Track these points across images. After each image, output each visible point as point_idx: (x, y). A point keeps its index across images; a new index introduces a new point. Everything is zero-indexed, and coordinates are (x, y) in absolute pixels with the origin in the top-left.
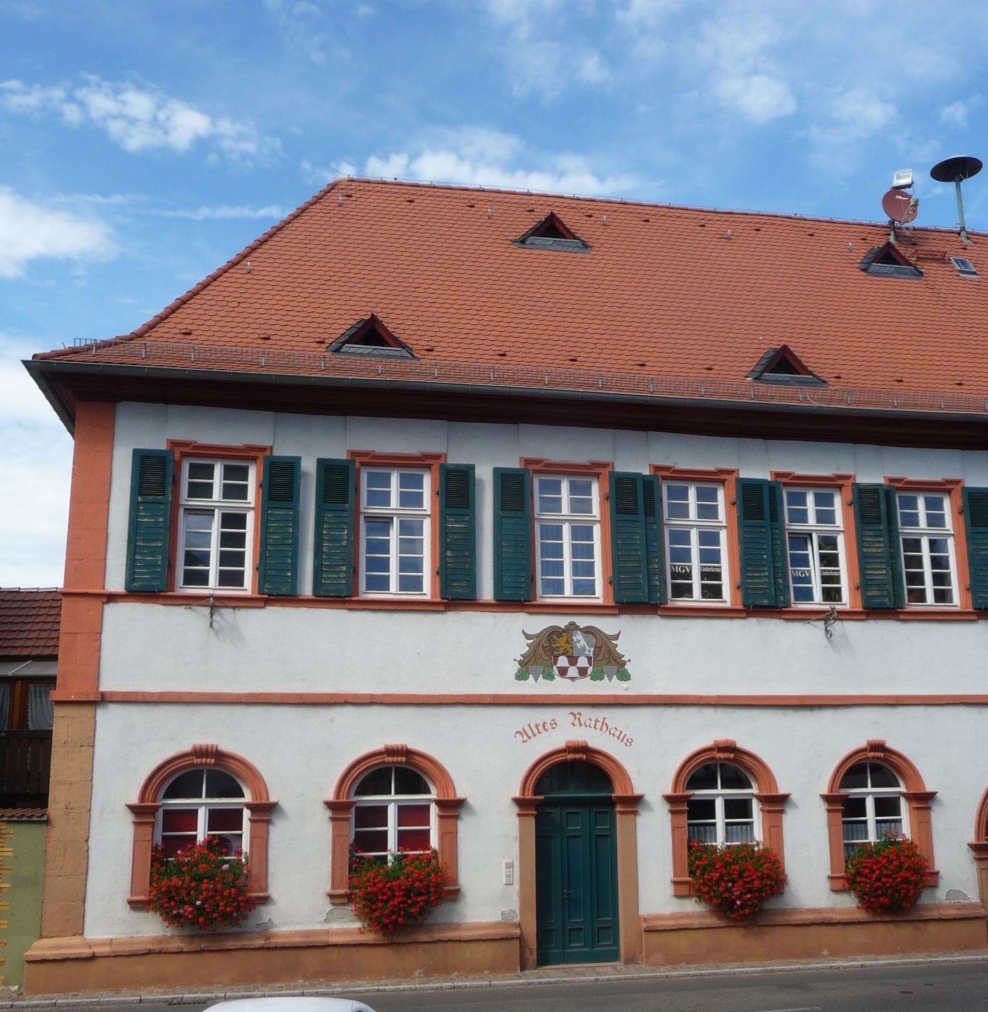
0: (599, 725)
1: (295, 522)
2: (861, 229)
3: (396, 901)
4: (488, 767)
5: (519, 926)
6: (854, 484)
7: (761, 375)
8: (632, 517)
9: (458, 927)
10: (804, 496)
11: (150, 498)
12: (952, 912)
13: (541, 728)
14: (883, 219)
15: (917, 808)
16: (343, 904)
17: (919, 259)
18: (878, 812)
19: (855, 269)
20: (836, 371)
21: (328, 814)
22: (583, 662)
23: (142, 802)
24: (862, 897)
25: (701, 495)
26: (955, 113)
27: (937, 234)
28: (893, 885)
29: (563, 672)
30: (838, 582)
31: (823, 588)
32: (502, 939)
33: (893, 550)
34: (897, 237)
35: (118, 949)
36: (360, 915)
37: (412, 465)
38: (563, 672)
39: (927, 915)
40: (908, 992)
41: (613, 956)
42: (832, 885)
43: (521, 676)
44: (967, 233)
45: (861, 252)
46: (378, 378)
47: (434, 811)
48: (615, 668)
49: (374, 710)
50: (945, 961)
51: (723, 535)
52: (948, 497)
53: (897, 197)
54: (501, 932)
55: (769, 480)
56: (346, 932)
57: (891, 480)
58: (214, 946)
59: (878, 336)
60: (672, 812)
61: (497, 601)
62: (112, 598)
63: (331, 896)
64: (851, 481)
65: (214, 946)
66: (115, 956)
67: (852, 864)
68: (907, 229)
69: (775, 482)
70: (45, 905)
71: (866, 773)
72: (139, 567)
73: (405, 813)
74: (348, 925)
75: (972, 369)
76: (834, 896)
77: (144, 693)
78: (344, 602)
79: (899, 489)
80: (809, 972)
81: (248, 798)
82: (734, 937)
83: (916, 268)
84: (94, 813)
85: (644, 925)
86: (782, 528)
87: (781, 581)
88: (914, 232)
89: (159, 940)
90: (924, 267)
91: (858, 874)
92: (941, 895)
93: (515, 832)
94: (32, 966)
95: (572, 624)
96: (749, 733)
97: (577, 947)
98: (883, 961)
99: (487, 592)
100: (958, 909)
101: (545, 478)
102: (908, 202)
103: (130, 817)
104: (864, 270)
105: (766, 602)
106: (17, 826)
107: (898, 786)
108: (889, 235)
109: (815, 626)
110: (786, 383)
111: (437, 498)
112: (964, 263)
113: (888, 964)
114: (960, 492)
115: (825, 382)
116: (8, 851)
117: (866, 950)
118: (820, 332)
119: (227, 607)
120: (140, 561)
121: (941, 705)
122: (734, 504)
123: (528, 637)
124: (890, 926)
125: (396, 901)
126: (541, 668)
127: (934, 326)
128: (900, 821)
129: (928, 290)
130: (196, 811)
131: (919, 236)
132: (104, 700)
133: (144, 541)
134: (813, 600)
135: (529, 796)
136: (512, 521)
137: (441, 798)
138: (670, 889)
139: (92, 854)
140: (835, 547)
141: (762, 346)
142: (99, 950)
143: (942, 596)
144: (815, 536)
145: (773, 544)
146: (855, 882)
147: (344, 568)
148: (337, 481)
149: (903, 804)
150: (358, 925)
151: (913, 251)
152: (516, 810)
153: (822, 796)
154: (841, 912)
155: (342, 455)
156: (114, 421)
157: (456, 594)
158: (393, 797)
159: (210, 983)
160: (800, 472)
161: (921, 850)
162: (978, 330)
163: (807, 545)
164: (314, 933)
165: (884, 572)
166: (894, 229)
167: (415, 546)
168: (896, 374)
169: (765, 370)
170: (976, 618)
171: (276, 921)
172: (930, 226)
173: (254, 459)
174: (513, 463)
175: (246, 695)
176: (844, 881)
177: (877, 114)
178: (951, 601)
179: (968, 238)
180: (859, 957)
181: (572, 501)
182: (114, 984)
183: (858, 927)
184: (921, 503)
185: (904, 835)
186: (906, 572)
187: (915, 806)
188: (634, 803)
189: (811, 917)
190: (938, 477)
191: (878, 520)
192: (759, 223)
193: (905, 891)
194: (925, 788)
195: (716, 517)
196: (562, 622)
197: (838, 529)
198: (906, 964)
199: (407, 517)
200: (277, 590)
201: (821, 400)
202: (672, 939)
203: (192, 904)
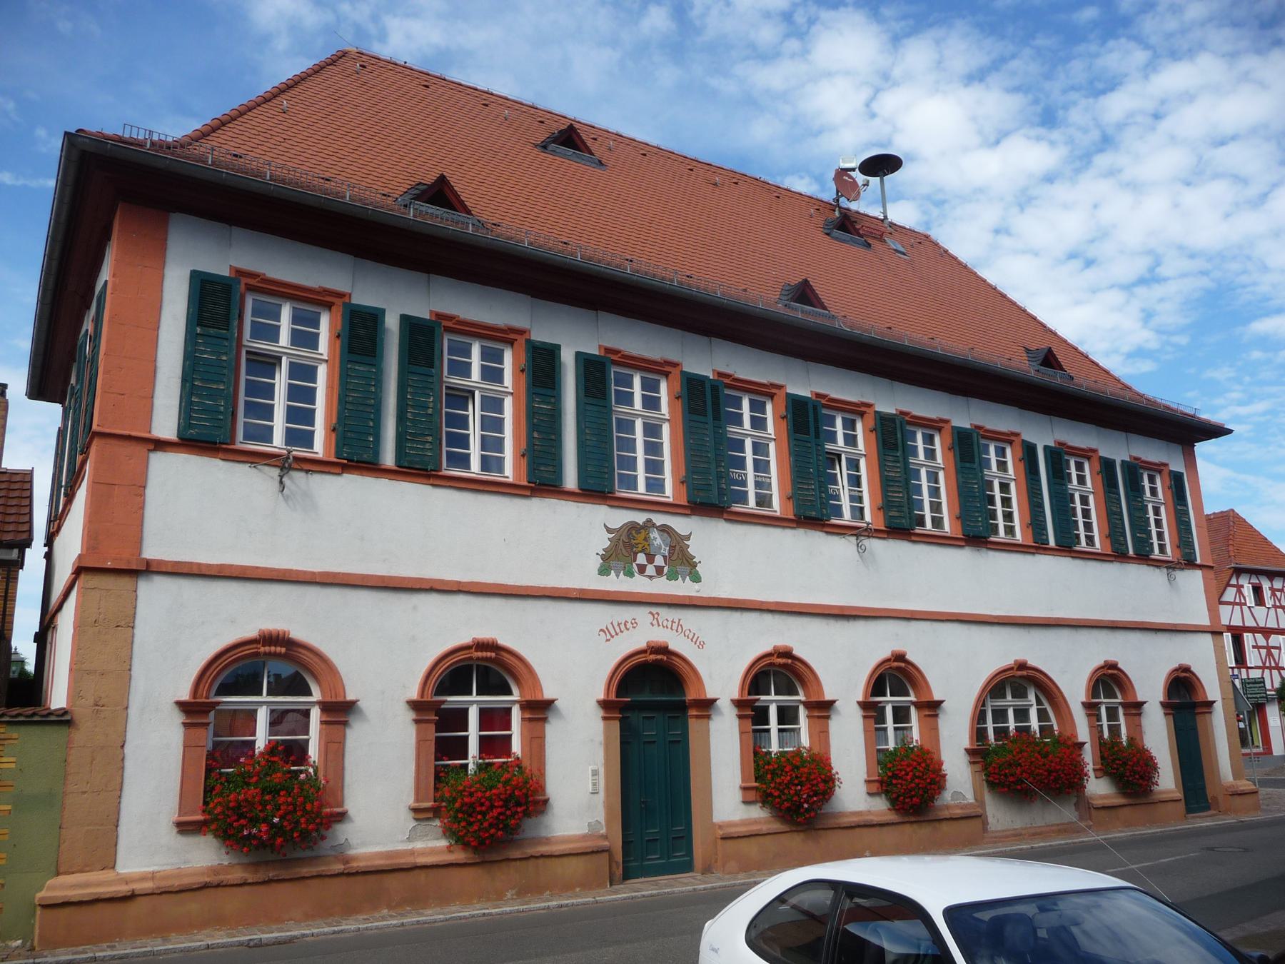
0: (675, 626)
1: (378, 380)
3: (495, 812)
4: (574, 663)
5: (605, 837)
8: (702, 419)
9: (547, 841)
11: (212, 331)
12: (958, 812)
13: (622, 627)
16: (428, 819)
21: (411, 715)
22: (659, 561)
29: (642, 569)
32: (593, 852)
35: (165, 884)
36: (448, 832)
37: (310, 301)
38: (642, 569)
41: (687, 867)
42: (744, 796)
43: (604, 571)
48: (688, 569)
49: (461, 599)
51: (322, 371)
54: (590, 845)
56: (433, 851)
58: (284, 874)
60: (740, 717)
62: (160, 445)
63: (415, 810)
65: (284, 874)
66: (161, 893)
70: (63, 831)
72: (197, 412)
73: (277, 719)
74: (432, 843)
77: (199, 565)
78: (429, 477)
81: (317, 695)
82: (796, 841)
84: (133, 712)
85: (721, 833)
86: (442, 381)
89: (214, 870)
91: (894, 776)
92: (947, 797)
93: (600, 737)
94: (49, 912)
95: (649, 521)
96: (806, 641)
97: (654, 859)
99: (571, 480)
103: (178, 718)
105: (813, 514)
106: (23, 729)
111: (338, 343)
116: (9, 762)
119: (301, 470)
120: (198, 404)
122: (522, 371)
123: (609, 530)
124: (915, 826)
125: (495, 812)
126: (621, 564)
130: (467, 710)
132: (149, 569)
133: (201, 380)
135: (613, 697)
136: (595, 408)
137: (328, 699)
138: (738, 795)
139: (128, 764)
142: (139, 887)
147: (430, 439)
148: (421, 339)
149: (802, 712)
150: (443, 843)
152: (601, 713)
156: (166, 233)
157: (541, 481)
158: (474, 697)
159: (279, 920)
164: (397, 854)
171: (353, 841)
173: (329, 306)
181: (484, 368)
182: (162, 929)
184: (476, 351)
188: (707, 705)
189: (855, 819)
190: (933, 416)
191: (895, 448)
194: (1135, 695)
196: (640, 518)
199: (492, 392)
200: (355, 456)
202: (743, 845)
203: (266, 820)
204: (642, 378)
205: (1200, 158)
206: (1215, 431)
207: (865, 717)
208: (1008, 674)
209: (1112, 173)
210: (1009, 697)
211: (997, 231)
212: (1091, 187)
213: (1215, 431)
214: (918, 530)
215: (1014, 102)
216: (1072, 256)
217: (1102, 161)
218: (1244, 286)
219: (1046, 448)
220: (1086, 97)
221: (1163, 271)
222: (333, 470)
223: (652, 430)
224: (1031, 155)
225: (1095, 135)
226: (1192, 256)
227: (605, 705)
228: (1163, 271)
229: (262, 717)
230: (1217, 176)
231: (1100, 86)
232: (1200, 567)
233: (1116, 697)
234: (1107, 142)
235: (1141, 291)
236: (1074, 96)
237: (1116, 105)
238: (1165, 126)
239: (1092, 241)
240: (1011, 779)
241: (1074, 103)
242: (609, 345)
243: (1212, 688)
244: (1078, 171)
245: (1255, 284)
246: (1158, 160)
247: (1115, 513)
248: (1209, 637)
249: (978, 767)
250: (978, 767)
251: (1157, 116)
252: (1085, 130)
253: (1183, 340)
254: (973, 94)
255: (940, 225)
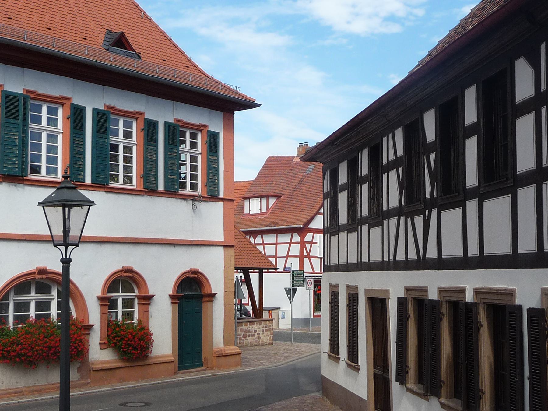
46: (53, 49)
47: (136, 301)
57: (28, 91)
60: (101, 305)
75: (20, 10)
78: (104, 188)
79: (32, 98)
99: (161, 188)
114: (69, 106)
148: (174, 133)
149: (136, 301)
153: (98, 297)
155: (19, 90)
160: (41, 91)
184: (44, 109)
204: (48, 107)
206: (249, 105)
207: (172, 303)
208: (30, 277)
210: (33, 293)
213: (249, 105)
214: (181, 192)
222: (89, 189)
223: (52, 137)
227: (172, 297)
229: (33, 305)
232: (222, 200)
240: (12, 354)
242: (178, 118)
243: (217, 283)
247: (150, 160)
248: (222, 249)
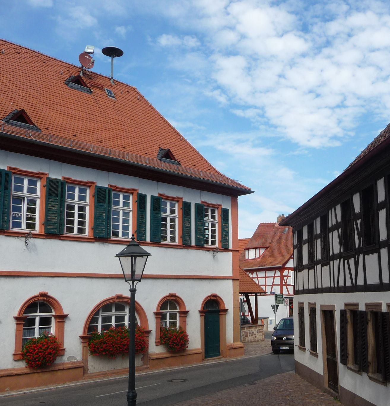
2: (68, 66)
6: (48, 178)
7: (9, 121)
10: (74, 188)
12: (69, 366)
14: (79, 65)
15: (59, 322)
17: (91, 85)
18: (41, 324)
19: (62, 83)
20: (74, 133)
23: (157, 311)
24: (28, 362)
25: (30, 183)
26: (121, 30)
27: (101, 77)
28: (44, 356)
30: (35, 221)
31: (27, 223)
33: (61, 209)
34: (83, 74)
39: (58, 368)
40: (43, 403)
42: (14, 358)
44: (113, 80)
45: (66, 76)
46: (126, 160)
47: (178, 315)
50: (63, 387)
52: (132, 195)
53: (86, 56)
55: (6, 170)
57: (65, 178)
59: (68, 115)
61: (196, 245)
64: (47, 176)
67: (25, 348)
68: (88, 71)
69: (9, 171)
71: (167, 304)
76: (15, 363)
79: (68, 183)
80: (154, 374)
83: (89, 89)
87: (6, 218)
88: (91, 73)
90: (93, 90)
91: (27, 352)
92: (65, 359)
98: (34, 390)
99: (193, 243)
100: (72, 364)
101: (115, 193)
102: (90, 60)
104: (67, 84)
107: (52, 312)
108: (80, 72)
109: (20, 240)
110: (21, 127)
112: (110, 92)
113: (37, 391)
114: (136, 194)
115: (41, 130)
117: (28, 386)
118: (42, 107)
121: (75, 277)
127: (93, 116)
128: (50, 328)
129: (93, 100)
131: (93, 76)
134: (21, 228)
140: (35, 205)
141: (12, 107)
143: (81, 231)
144: (25, 198)
145: (4, 200)
146: (26, 356)
148: (201, 210)
149: (53, 321)
151: (90, 81)
154: (18, 370)
158: (168, 311)
160: (208, 202)
161: (58, 340)
162: (112, 121)
163: (21, 203)
165: (56, 218)
166: (83, 70)
167: (33, 211)
168: (74, 133)
169: (11, 119)
170: (183, 248)
172: (99, 73)
174: (156, 195)
175: (108, 275)
176: (21, 356)
177: (89, 21)
178: (85, 233)
179: (114, 82)
180: (24, 389)
183: (25, 376)
184: (77, 190)
185: (51, 334)
186: (67, 219)
187: (58, 321)
190: (85, 180)
191: (57, 195)
192: (20, 50)
193: (49, 358)
195: (85, 200)
197: (176, 216)
198: (45, 390)
201: (37, 138)
205: (365, 56)
208: (112, 301)
209: (329, 57)
210: (114, 311)
211: (280, 76)
212: (320, 62)
215: (292, 18)
216: (311, 92)
217: (326, 51)
218: (377, 114)
219: (152, 197)
220: (321, 21)
221: (347, 103)
224: (295, 44)
225: (324, 39)
226: (358, 98)
227: (200, 312)
228: (347, 103)
230: (370, 65)
231: (327, 17)
232: (231, 251)
233: (177, 309)
234: (328, 44)
235: (338, 110)
236: (316, 20)
237: (334, 27)
238: (352, 40)
239: (319, 86)
241: (316, 23)
244: (316, 54)
245: (381, 113)
246: (348, 55)
247: (186, 227)
249: (86, 344)
250: (86, 344)
251: (350, 36)
252: (320, 36)
253: (352, 134)
254: (273, 11)
255: (254, 70)
